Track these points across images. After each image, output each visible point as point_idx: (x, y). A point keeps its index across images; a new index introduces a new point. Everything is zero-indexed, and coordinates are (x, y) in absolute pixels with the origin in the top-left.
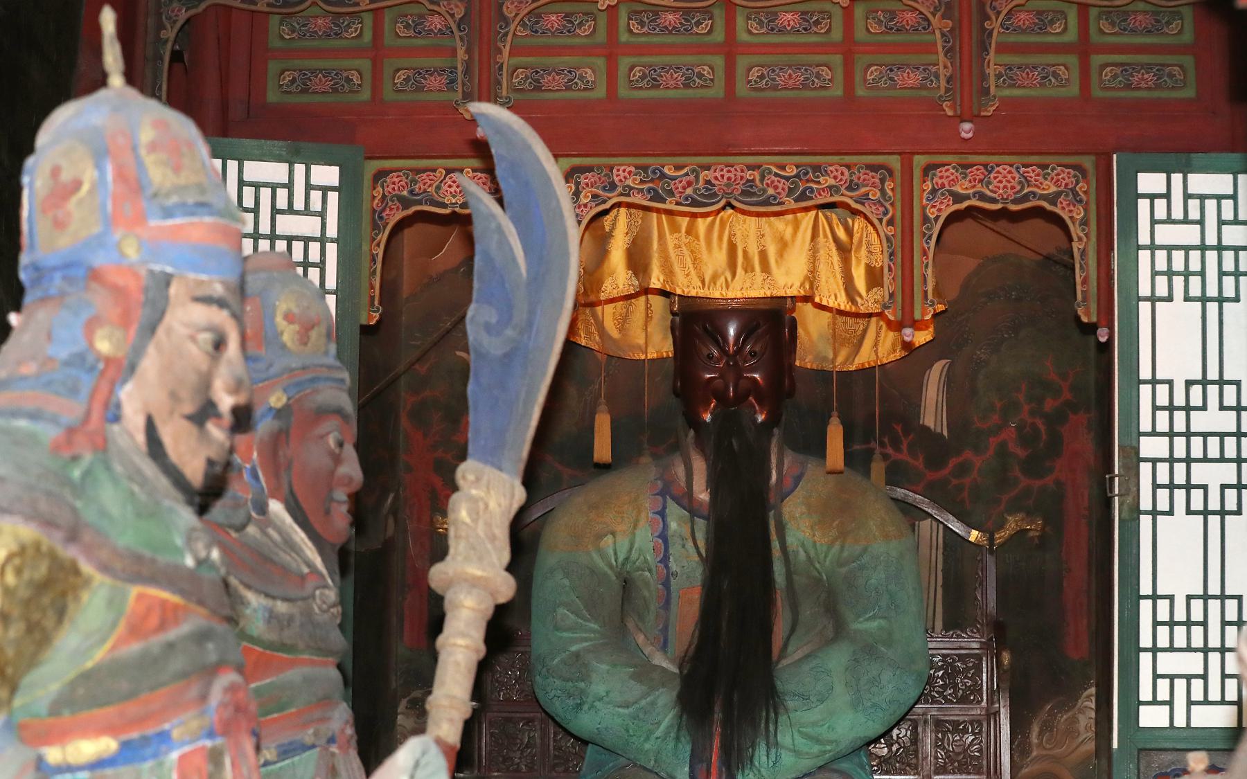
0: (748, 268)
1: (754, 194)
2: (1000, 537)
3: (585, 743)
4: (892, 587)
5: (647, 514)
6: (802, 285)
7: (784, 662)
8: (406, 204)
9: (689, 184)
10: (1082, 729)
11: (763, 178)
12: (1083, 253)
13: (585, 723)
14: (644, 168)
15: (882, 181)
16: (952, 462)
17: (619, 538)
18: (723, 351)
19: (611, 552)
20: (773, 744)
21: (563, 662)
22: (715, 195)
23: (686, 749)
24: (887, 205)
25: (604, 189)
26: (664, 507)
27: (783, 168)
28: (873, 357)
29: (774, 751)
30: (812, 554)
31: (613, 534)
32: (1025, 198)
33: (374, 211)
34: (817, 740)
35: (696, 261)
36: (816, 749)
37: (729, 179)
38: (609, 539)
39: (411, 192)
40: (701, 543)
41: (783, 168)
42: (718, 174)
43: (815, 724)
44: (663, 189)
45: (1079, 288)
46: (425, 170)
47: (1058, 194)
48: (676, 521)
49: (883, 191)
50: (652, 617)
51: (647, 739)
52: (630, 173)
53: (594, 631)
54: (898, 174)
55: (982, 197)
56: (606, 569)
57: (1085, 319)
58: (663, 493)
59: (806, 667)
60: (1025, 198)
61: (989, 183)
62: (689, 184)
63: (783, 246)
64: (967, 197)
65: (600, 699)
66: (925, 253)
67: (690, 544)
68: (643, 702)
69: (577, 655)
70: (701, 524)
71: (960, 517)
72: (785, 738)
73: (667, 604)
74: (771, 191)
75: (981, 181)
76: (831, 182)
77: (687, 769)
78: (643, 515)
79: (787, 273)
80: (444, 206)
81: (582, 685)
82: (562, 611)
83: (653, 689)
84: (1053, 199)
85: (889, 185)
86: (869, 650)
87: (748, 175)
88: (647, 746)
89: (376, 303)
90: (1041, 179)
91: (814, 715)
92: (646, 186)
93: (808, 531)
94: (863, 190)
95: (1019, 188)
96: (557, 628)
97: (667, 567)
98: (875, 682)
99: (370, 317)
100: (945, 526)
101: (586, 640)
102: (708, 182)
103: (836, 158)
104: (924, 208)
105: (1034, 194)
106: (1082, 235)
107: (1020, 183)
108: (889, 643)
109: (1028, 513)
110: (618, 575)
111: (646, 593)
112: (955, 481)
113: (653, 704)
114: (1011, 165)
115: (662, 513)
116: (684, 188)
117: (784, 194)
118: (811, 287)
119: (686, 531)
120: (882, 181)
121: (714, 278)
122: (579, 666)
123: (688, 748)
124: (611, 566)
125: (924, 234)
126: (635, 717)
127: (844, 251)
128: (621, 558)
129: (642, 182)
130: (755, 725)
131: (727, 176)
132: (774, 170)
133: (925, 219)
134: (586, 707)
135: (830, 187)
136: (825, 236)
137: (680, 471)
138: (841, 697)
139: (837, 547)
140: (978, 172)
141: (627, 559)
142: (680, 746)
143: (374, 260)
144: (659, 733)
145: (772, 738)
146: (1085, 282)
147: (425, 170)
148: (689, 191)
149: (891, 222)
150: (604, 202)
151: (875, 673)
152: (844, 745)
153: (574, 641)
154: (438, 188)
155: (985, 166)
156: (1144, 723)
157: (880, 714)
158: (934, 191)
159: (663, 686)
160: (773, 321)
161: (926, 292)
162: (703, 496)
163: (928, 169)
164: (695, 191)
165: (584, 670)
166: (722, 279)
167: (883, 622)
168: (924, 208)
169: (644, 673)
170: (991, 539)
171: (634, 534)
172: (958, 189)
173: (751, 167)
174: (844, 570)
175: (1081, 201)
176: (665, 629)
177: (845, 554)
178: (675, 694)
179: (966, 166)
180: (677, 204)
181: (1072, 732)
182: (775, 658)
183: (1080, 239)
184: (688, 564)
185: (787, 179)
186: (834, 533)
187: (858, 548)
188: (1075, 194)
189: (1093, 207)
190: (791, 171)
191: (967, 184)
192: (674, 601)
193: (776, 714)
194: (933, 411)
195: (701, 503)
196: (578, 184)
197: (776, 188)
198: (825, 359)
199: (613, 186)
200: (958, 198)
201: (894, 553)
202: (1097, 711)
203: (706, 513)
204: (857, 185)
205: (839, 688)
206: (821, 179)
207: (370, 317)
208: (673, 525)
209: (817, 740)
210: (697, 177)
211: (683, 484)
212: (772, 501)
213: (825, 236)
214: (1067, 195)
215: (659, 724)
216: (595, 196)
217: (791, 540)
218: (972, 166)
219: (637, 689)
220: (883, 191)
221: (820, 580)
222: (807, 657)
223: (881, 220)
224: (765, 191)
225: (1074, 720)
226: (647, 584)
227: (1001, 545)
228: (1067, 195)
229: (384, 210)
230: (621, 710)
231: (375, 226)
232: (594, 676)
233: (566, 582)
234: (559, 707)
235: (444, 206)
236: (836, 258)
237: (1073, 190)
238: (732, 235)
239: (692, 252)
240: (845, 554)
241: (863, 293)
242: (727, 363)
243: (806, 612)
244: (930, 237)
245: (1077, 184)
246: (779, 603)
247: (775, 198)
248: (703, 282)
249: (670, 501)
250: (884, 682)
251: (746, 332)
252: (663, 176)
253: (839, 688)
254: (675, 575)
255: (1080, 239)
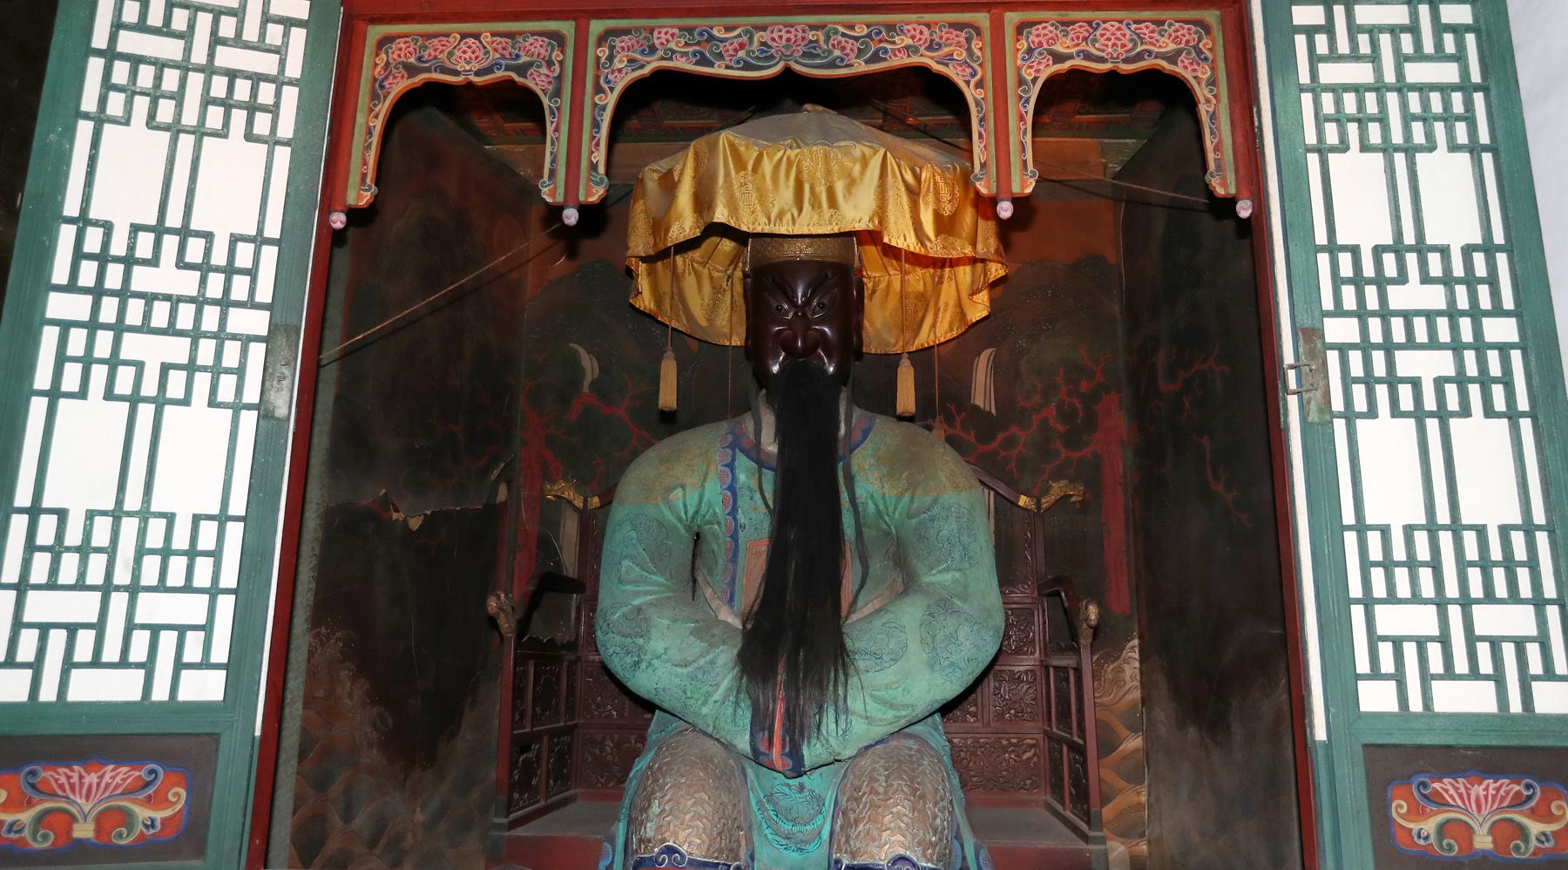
0: (816, 204)
1: (818, 56)
2: (1046, 502)
3: (649, 707)
4: (965, 538)
5: (717, 466)
6: (871, 220)
7: (854, 617)
8: (411, 70)
9: (742, 46)
10: (1128, 678)
11: (828, 38)
12: (1213, 117)
13: (644, 682)
14: (690, 30)
15: (968, 40)
16: (1000, 436)
17: (688, 489)
18: (793, 304)
19: (681, 506)
20: (842, 710)
21: (624, 616)
22: (772, 57)
23: (745, 715)
24: (975, 65)
25: (642, 52)
26: (733, 460)
27: (852, 27)
28: (932, 337)
29: (843, 717)
30: (881, 507)
31: (683, 487)
32: (1139, 57)
33: (375, 80)
34: (890, 705)
35: (762, 198)
36: (890, 714)
37: (788, 40)
38: (679, 492)
39: (419, 59)
40: (771, 503)
41: (852, 27)
42: (775, 35)
43: (888, 687)
44: (711, 52)
45: (1211, 156)
46: (436, 35)
47: (1179, 52)
48: (745, 472)
49: (969, 50)
50: (719, 570)
51: (705, 702)
52: (673, 35)
53: (659, 585)
54: (987, 34)
55: (1088, 56)
56: (675, 521)
57: (1220, 191)
58: (732, 447)
59: (878, 623)
60: (1139, 57)
61: (1095, 41)
62: (742, 46)
63: (851, 184)
64: (1070, 57)
65: (659, 657)
66: (1022, 118)
67: (758, 496)
68: (702, 662)
69: (639, 609)
70: (769, 477)
71: (1008, 484)
72: (855, 702)
73: (734, 558)
74: (837, 53)
75: (1085, 39)
76: (909, 41)
77: (747, 737)
78: (713, 468)
79: (855, 207)
80: (456, 73)
81: (641, 641)
82: (626, 563)
83: (712, 646)
84: (1172, 58)
85: (976, 45)
86: (943, 604)
87: (811, 35)
88: (705, 710)
89: (368, 181)
90: (1156, 35)
91: (887, 676)
92: (691, 49)
93: (877, 483)
94: (946, 50)
95: (1130, 45)
96: (620, 581)
97: (735, 519)
98: (952, 638)
99: (360, 197)
100: (996, 493)
101: (646, 593)
102: (764, 44)
103: (913, 17)
104: (1018, 69)
105: (1150, 53)
106: (1209, 96)
107: (1132, 40)
108: (965, 597)
109: (1071, 481)
110: (688, 528)
111: (715, 547)
112: (1003, 454)
113: (712, 662)
114: (1120, 22)
115: (731, 466)
116: (736, 50)
117: (853, 55)
118: (880, 223)
119: (754, 484)
120: (968, 40)
121: (780, 216)
122: (639, 620)
123: (748, 714)
124: (680, 520)
125: (1021, 97)
126: (693, 678)
127: (913, 194)
128: (691, 510)
129: (686, 44)
130: (821, 686)
131: (785, 36)
132: (841, 29)
133: (1021, 82)
134: (643, 665)
135: (907, 48)
136: (894, 175)
137: (749, 425)
138: (916, 655)
139: (906, 499)
140: (1083, 30)
141: (697, 512)
142: (740, 712)
143: (370, 133)
144: (716, 697)
145: (841, 703)
146: (1217, 148)
147: (436, 35)
148: (741, 54)
149: (980, 85)
150: (642, 67)
151: (951, 629)
152: (921, 710)
153: (637, 594)
154: (451, 54)
155: (1090, 23)
156: (1365, 706)
157: (959, 674)
158: (1030, 51)
159: (724, 642)
160: (838, 272)
161: (1025, 162)
162: (771, 447)
163: (1021, 29)
164: (748, 54)
165: (644, 626)
166: (789, 216)
167: (957, 575)
168: (1018, 69)
169: (706, 629)
170: (1038, 504)
171: (703, 486)
172: (1058, 48)
173: (813, 27)
174: (914, 521)
175: (1206, 59)
176: (732, 582)
177: (915, 506)
178: (735, 651)
179: (1066, 24)
180: (727, 67)
181: (1118, 681)
182: (843, 614)
183: (1208, 101)
184: (756, 518)
185: (856, 39)
186: (903, 484)
187: (928, 500)
188: (1199, 52)
189: (1221, 65)
190: (861, 31)
191: (1069, 43)
192: (742, 553)
193: (846, 675)
194: (982, 393)
195: (768, 454)
196: (612, 48)
197: (843, 48)
198: (888, 344)
199: (653, 49)
200: (1058, 58)
201: (964, 504)
202: (1141, 662)
203: (774, 464)
204: (939, 45)
205: (914, 646)
206: (897, 39)
207: (360, 197)
208: (742, 477)
209: (890, 705)
210: (751, 39)
211: (752, 437)
212: (841, 452)
213: (894, 175)
214: (1189, 53)
215: (718, 685)
216: (631, 61)
217: (861, 491)
218: (1074, 23)
219: (698, 646)
220: (969, 50)
221: (889, 533)
222: (878, 611)
223: (968, 83)
224: (830, 53)
225: (1120, 670)
226: (716, 537)
227: (1048, 509)
228: (1189, 53)
229: (386, 78)
230: (679, 670)
231: (374, 96)
232: (653, 631)
233: (633, 534)
234: (619, 665)
235: (456, 73)
236: (905, 198)
237: (1196, 48)
238: (799, 173)
239: (758, 189)
240: (915, 506)
241: (932, 236)
242: (796, 314)
243: (876, 566)
244: (1027, 101)
245: (1200, 40)
246: (848, 555)
247: (842, 60)
248: (769, 219)
249: (740, 455)
250: (962, 639)
251: (815, 288)
252: (711, 38)
253: (914, 646)
254: (743, 527)
255: (1208, 101)
